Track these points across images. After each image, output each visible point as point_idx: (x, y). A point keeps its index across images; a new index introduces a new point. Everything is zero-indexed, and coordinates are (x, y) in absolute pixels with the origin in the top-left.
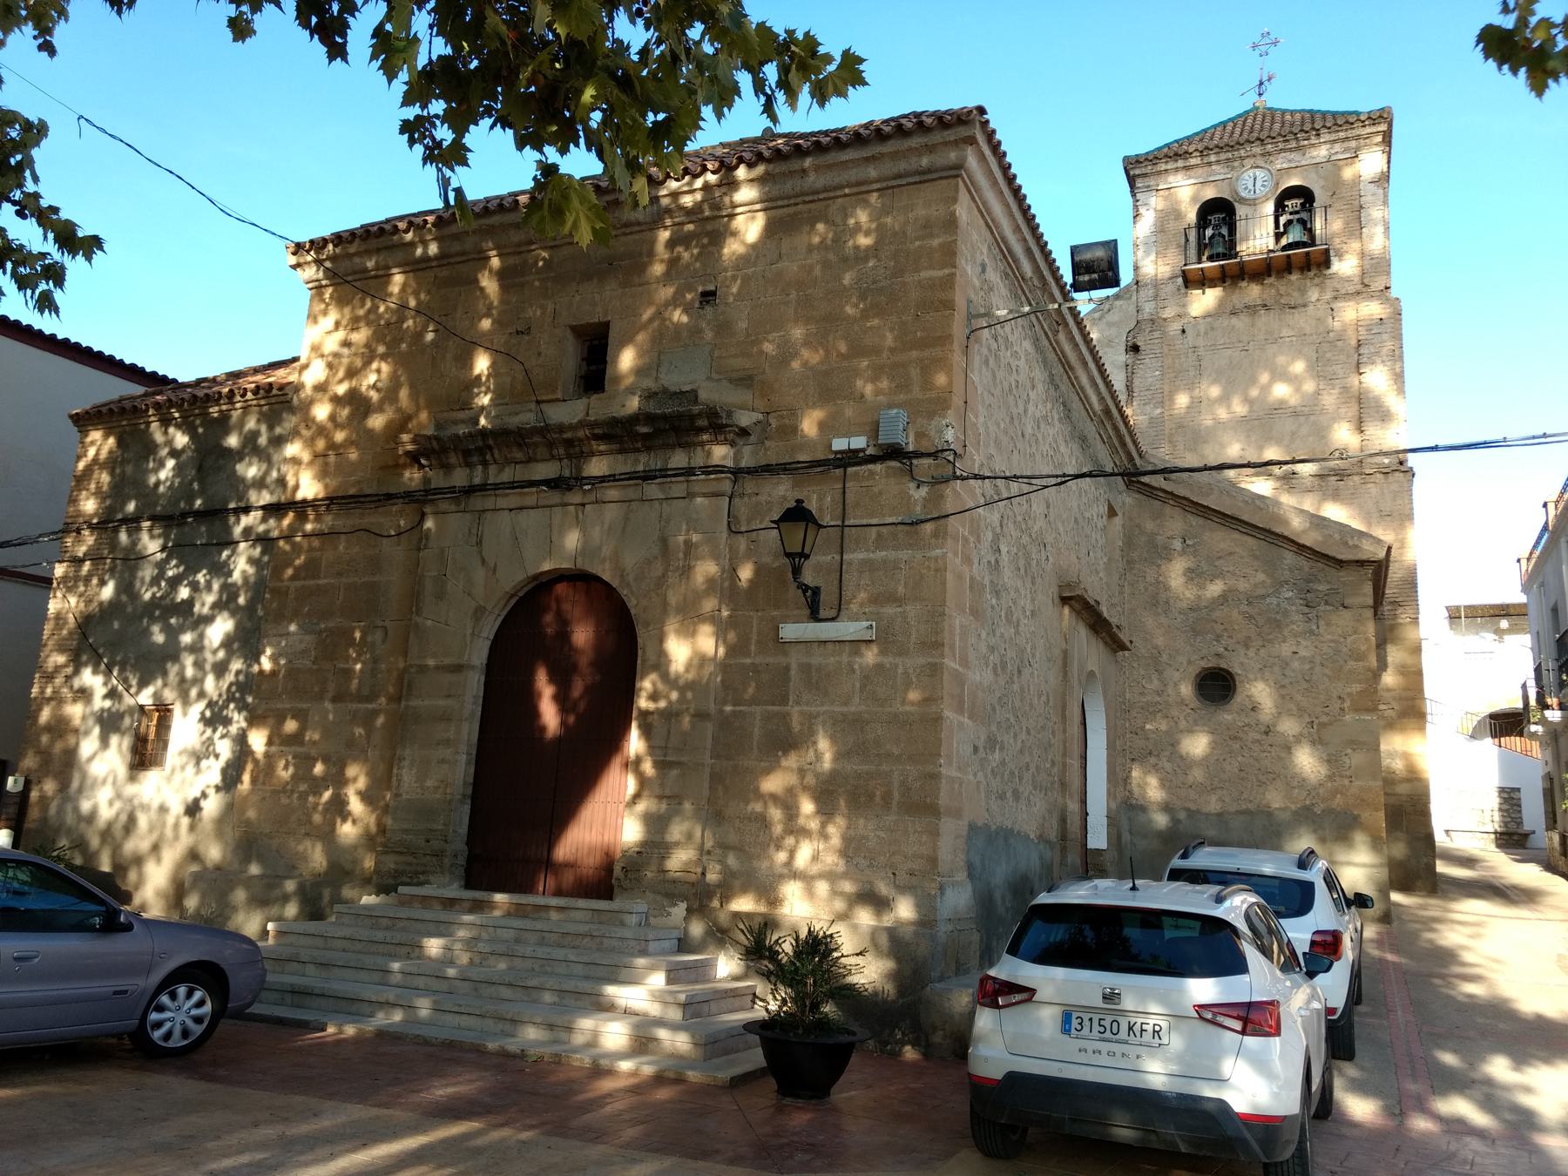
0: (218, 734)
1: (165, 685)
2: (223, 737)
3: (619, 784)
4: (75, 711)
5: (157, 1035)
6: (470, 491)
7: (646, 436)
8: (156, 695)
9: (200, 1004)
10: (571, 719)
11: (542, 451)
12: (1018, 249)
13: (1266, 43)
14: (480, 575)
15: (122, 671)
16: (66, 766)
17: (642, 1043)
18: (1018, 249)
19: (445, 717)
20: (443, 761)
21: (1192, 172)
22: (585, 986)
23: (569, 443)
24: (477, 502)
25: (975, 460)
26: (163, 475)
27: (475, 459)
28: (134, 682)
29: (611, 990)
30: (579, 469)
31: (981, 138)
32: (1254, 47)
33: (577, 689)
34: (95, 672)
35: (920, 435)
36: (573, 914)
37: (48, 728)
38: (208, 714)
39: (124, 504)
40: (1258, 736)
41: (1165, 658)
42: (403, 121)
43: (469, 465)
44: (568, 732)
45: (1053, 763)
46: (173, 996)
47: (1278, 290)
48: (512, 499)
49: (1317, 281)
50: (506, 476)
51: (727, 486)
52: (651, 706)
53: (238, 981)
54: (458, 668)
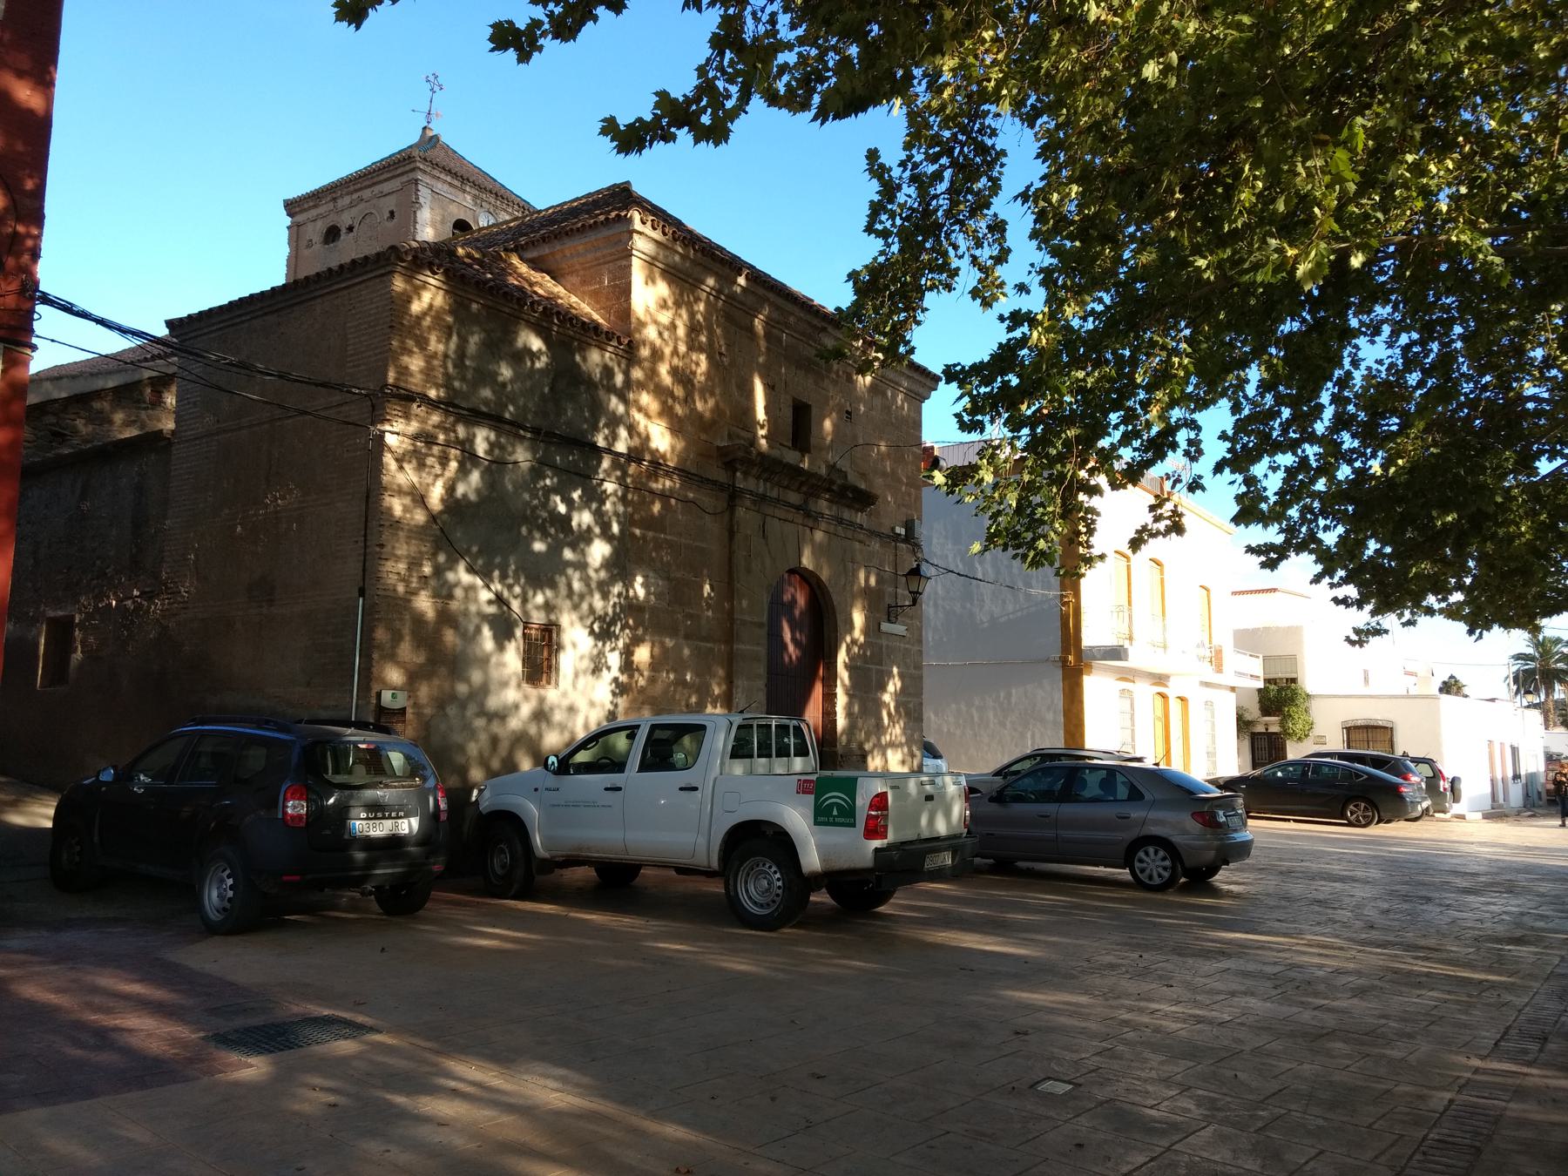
0: (608, 647)
2: (613, 650)
38: (596, 627)
42: (293, 207)
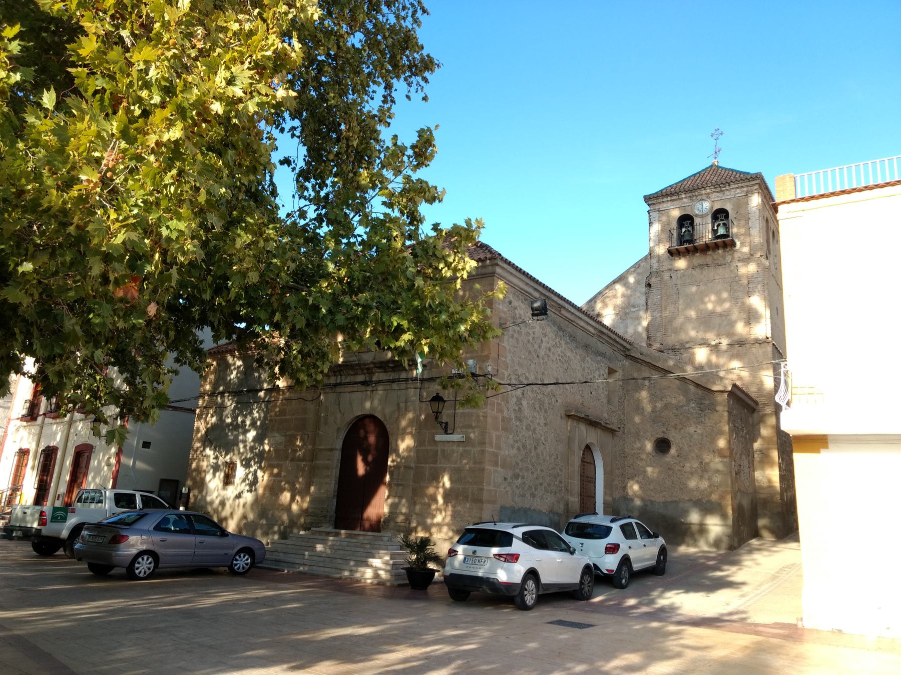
1: (234, 455)
3: (384, 492)
4: (204, 464)
5: (236, 568)
6: (336, 385)
7: (392, 367)
8: (231, 458)
9: (247, 560)
10: (368, 468)
11: (360, 372)
12: (530, 290)
13: (717, 134)
14: (339, 416)
15: (219, 449)
16: (201, 485)
17: (377, 576)
18: (530, 290)
19: (327, 467)
20: (327, 483)
21: (674, 203)
22: (363, 559)
23: (368, 369)
24: (338, 389)
25: (506, 375)
26: (233, 376)
27: (337, 374)
28: (223, 453)
29: (371, 560)
30: (372, 378)
31: (500, 263)
32: (712, 135)
33: (370, 458)
34: (210, 450)
35: (480, 368)
36: (367, 537)
37: (195, 470)
39: (219, 387)
40: (679, 468)
41: (641, 433)
43: (335, 375)
44: (367, 474)
45: (561, 482)
46: (240, 557)
47: (713, 257)
48: (349, 388)
49: (730, 253)
50: (348, 380)
51: (419, 385)
52: (392, 464)
53: (258, 553)
54: (331, 450)
